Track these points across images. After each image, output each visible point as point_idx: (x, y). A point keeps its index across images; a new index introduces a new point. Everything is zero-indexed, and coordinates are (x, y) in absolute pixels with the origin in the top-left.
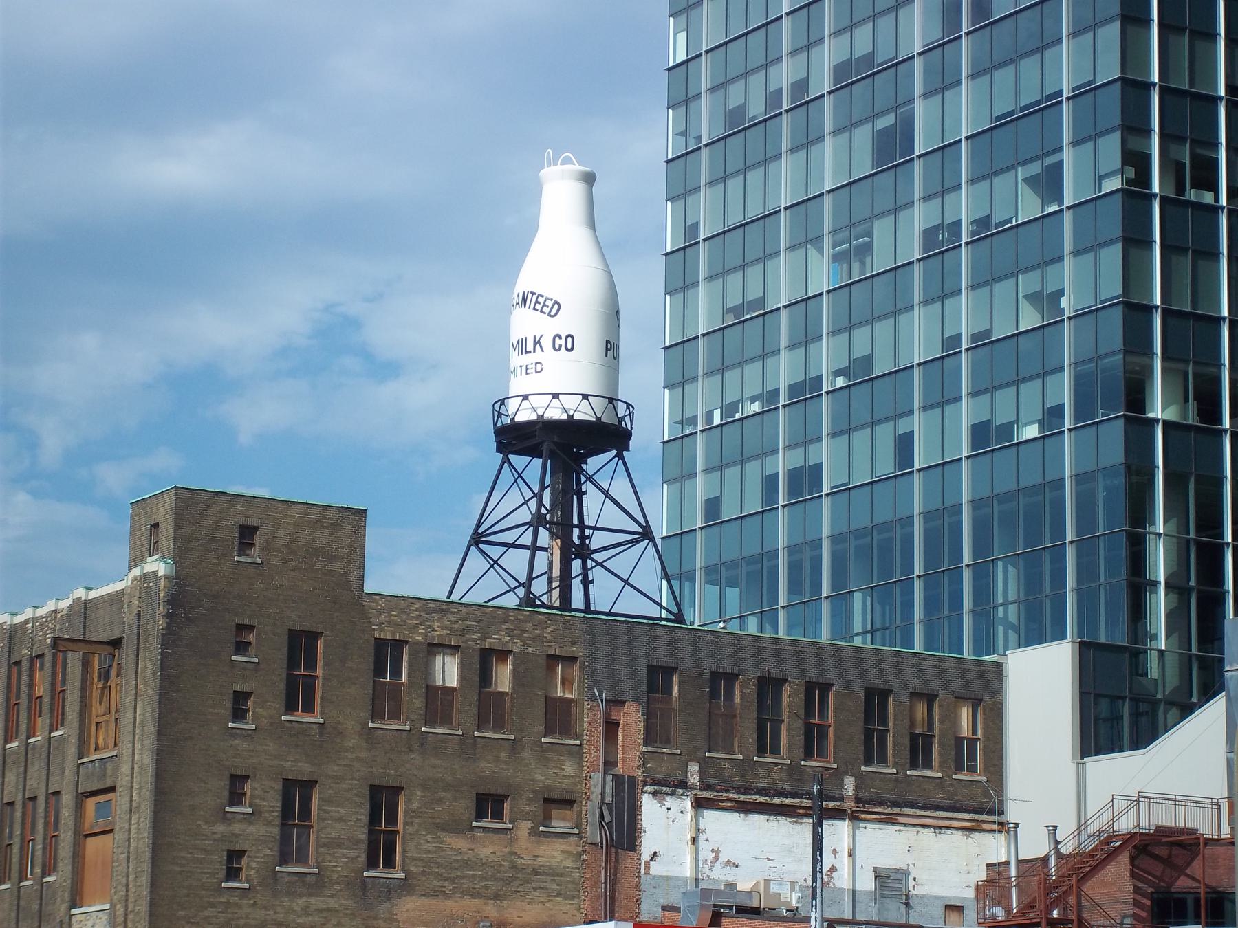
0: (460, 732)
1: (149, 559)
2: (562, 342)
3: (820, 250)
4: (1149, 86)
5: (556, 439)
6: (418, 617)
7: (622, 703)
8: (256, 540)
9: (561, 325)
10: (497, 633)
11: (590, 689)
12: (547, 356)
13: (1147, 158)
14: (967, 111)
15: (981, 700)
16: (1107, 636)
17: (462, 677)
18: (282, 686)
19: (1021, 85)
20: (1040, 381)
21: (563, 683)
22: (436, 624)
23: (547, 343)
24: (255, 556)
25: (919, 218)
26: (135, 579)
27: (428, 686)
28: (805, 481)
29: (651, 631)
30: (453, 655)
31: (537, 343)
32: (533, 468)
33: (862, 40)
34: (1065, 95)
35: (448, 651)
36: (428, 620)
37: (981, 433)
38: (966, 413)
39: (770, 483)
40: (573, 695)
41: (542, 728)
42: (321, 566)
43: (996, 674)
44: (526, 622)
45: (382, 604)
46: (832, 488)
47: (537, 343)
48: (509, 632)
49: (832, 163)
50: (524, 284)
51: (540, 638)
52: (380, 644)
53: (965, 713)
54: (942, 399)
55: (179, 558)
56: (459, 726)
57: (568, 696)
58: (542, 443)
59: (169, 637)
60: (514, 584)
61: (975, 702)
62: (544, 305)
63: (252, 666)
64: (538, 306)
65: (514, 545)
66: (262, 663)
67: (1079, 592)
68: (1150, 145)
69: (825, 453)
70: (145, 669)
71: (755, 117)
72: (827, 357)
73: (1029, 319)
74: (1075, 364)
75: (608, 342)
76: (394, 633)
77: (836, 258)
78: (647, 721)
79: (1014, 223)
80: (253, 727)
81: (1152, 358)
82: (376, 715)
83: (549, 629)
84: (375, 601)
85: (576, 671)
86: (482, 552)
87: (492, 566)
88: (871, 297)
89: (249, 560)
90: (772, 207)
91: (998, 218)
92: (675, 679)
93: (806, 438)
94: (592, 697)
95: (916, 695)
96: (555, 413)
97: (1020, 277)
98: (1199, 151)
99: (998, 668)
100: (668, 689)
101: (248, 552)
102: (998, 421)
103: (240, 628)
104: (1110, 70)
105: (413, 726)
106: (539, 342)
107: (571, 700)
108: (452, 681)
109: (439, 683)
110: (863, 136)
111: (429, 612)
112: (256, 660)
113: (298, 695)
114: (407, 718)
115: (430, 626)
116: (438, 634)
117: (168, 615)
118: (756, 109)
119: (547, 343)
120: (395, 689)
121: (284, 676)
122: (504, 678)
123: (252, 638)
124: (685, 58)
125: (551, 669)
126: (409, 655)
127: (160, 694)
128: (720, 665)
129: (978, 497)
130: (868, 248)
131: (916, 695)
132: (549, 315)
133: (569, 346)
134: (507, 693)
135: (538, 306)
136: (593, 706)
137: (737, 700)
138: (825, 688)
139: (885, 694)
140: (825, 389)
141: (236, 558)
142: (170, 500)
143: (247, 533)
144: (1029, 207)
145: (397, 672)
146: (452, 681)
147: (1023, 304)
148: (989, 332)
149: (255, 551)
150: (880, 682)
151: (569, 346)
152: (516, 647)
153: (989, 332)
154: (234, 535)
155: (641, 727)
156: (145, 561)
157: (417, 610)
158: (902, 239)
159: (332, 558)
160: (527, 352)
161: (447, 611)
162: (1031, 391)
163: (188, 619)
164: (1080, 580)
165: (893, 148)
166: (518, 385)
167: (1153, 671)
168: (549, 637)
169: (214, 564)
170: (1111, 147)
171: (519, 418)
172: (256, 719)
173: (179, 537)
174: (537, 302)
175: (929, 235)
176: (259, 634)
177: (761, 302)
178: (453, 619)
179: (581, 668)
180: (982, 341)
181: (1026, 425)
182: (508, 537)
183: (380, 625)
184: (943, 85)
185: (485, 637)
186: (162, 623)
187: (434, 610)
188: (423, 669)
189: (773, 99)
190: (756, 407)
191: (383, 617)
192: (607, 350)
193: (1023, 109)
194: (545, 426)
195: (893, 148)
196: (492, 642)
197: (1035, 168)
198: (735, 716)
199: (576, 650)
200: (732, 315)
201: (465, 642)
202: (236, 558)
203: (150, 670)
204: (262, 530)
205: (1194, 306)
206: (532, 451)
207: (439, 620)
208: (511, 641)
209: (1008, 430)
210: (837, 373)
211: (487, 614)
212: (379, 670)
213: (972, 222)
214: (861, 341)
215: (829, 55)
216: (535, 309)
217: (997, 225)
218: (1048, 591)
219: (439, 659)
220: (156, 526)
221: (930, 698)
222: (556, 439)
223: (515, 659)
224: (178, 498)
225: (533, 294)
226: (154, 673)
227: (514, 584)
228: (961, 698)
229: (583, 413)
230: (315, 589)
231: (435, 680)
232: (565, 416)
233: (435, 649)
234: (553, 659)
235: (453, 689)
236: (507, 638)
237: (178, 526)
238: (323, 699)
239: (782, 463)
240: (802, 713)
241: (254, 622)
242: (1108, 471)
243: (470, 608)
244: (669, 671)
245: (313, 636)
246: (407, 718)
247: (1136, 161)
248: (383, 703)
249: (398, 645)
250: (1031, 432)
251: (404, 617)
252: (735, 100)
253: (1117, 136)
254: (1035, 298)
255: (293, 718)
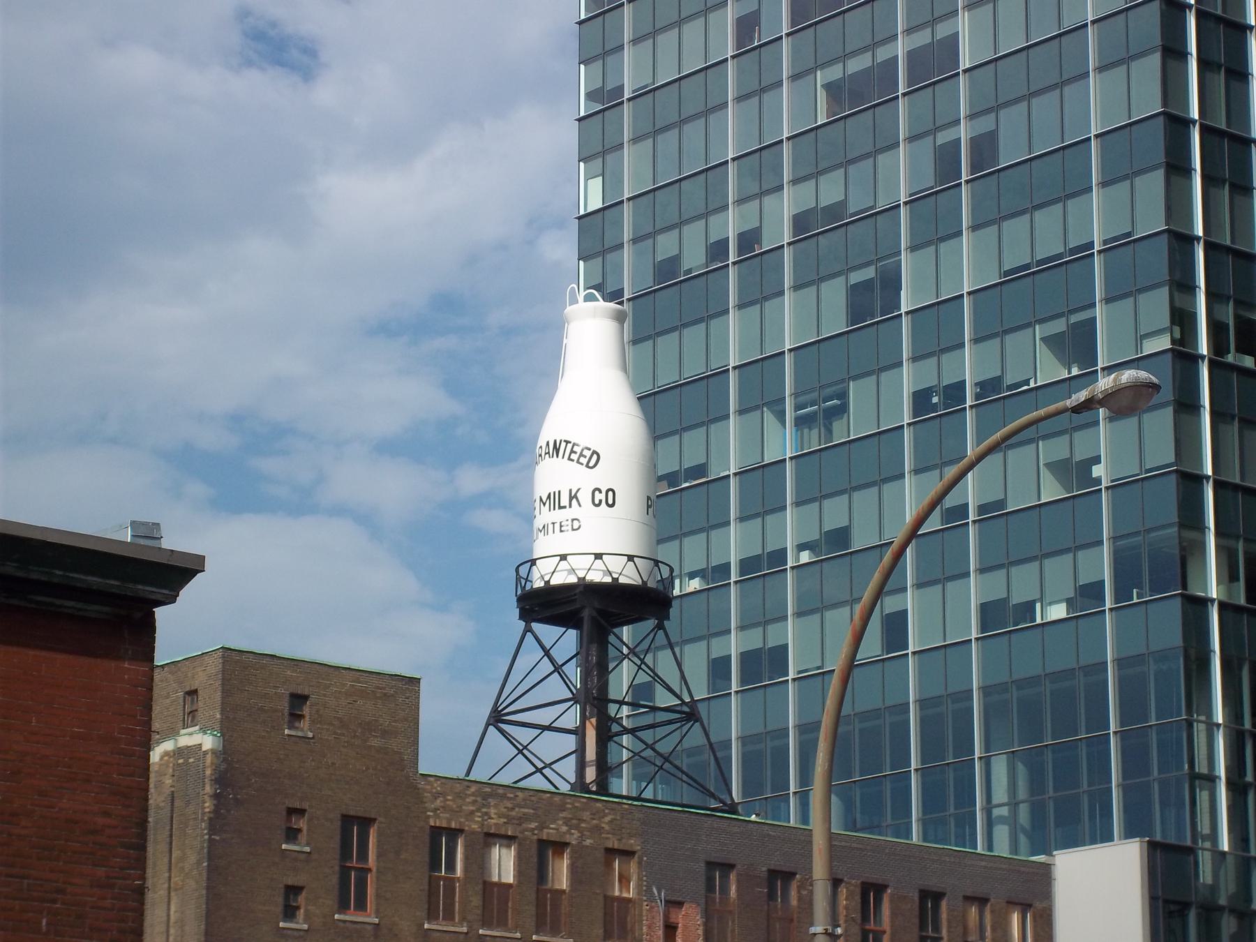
0: (518, 935)
1: (183, 732)
2: (603, 496)
3: (781, 416)
4: (1193, 239)
5: (597, 605)
6: (474, 802)
7: (680, 904)
8: (306, 710)
9: (602, 477)
10: (554, 822)
11: (649, 890)
12: (585, 511)
13: (1193, 317)
14: (969, 265)
15: (1030, 906)
16: (1163, 831)
17: (519, 872)
18: (335, 880)
19: (1044, 234)
20: (1071, 555)
21: (620, 881)
22: (493, 811)
23: (585, 496)
24: (305, 728)
25: (908, 379)
26: (166, 754)
27: (485, 883)
28: (765, 665)
29: (709, 821)
30: (509, 847)
31: (573, 497)
32: (566, 641)
33: (830, 190)
34: (1097, 248)
35: (505, 842)
36: (484, 806)
37: (991, 614)
38: (975, 591)
39: (719, 669)
40: (631, 894)
41: (601, 931)
42: (375, 742)
43: (1044, 875)
44: (583, 810)
45: (437, 787)
46: (800, 672)
47: (573, 497)
48: (567, 822)
49: (792, 321)
50: (548, 434)
51: (598, 829)
52: (436, 832)
53: (1015, 918)
54: (941, 574)
55: (227, 729)
56: (516, 929)
57: (625, 895)
58: (583, 608)
59: (216, 823)
60: (547, 771)
61: (1025, 907)
62: (581, 455)
63: (303, 857)
64: (574, 457)
65: (549, 728)
66: (312, 844)
67: (1126, 789)
68: (1194, 303)
69: (790, 633)
70: (182, 858)
71: (690, 271)
72: (791, 529)
73: (1051, 491)
74: (1114, 539)
75: (649, 498)
76: (449, 820)
77: (800, 422)
78: (706, 924)
79: (1032, 385)
80: (305, 927)
81: (1204, 533)
82: (432, 915)
83: (608, 819)
84: (429, 783)
85: (633, 867)
86: (502, 732)
87: (525, 747)
88: (845, 467)
89: (300, 734)
90: (715, 364)
91: (1009, 380)
92: (733, 877)
93: (764, 616)
94: (651, 899)
95: (970, 899)
96: (597, 576)
97: (1041, 443)
98: (1242, 313)
99: (1046, 870)
100: (725, 890)
101: (297, 724)
102: (1015, 600)
103: (291, 811)
104: (1153, 221)
105: (470, 927)
106: (575, 496)
107: (629, 900)
108: (509, 878)
109: (495, 879)
110: (835, 294)
111: (486, 796)
112: (307, 849)
113: (349, 891)
114: (463, 919)
115: (486, 814)
116: (495, 822)
117: (216, 796)
118: (694, 259)
119: (585, 496)
120: (450, 882)
121: (337, 868)
122: (561, 874)
123: (302, 824)
124: (600, 205)
125: (609, 865)
126: (466, 847)
127: (208, 888)
128: (777, 862)
129: (988, 683)
130: (842, 409)
131: (970, 899)
132: (587, 466)
133: (610, 502)
134: (563, 892)
135: (573, 456)
136: (652, 907)
137: (794, 902)
138: (880, 889)
139: (938, 896)
140: (790, 564)
141: (286, 732)
142: (214, 665)
143: (298, 699)
144: (1050, 370)
145: (451, 866)
146: (509, 878)
147: (1046, 475)
148: (1001, 504)
149: (304, 724)
150: (933, 883)
151: (610, 502)
152: (573, 838)
153: (1001, 504)
154: (285, 705)
155: (700, 932)
156: (178, 734)
157: (473, 794)
158: (885, 402)
159: (385, 733)
160: (560, 507)
161: (503, 797)
162: (1058, 570)
163: (236, 799)
164: (1126, 773)
165: (873, 301)
166: (544, 546)
167: (1206, 874)
168: (607, 827)
169: (263, 737)
170: (1157, 305)
171: (556, 581)
172: (307, 918)
173: (226, 708)
174: (572, 452)
175: (921, 400)
176: (310, 820)
177: (700, 470)
178: (510, 805)
179: (640, 863)
180: (991, 511)
181: (1050, 604)
182: (543, 716)
183: (435, 810)
184: (937, 232)
185: (542, 827)
186: (209, 805)
187: (490, 795)
188: (478, 862)
189: (718, 250)
190: (695, 584)
191: (438, 802)
192: (649, 507)
193: (1040, 263)
194: (587, 589)
195: (873, 301)
196: (549, 833)
197: (1059, 326)
198: (792, 920)
199: (633, 843)
200: (665, 483)
201: (522, 832)
202: (286, 732)
203: (193, 858)
204: (313, 698)
205: (1242, 479)
206: (565, 620)
207: (496, 806)
208: (569, 832)
209: (1027, 609)
210: (801, 547)
211: (546, 803)
212: (434, 864)
213: (976, 384)
214: (834, 514)
215: (787, 204)
216: (569, 459)
217: (1010, 388)
218: (1085, 786)
219: (496, 851)
220: (193, 693)
221: (982, 901)
222: (597, 605)
223: (573, 852)
224: (225, 660)
225: (567, 442)
226: (199, 863)
227: (547, 771)
228: (1011, 903)
229: (629, 576)
230: (368, 769)
231: (490, 876)
232: (608, 580)
233: (491, 840)
234: (611, 852)
235: (510, 886)
236: (564, 828)
237: (226, 693)
238: (378, 896)
239: (734, 645)
240: (857, 916)
241: (306, 806)
242: (1162, 656)
243: (527, 794)
244: (727, 867)
245: (366, 822)
246: (463, 919)
247: (1182, 319)
248: (436, 900)
249: (453, 834)
250: (1058, 612)
251: (459, 802)
252: (666, 245)
253: (1164, 292)
254: (1061, 469)
255: (347, 918)
